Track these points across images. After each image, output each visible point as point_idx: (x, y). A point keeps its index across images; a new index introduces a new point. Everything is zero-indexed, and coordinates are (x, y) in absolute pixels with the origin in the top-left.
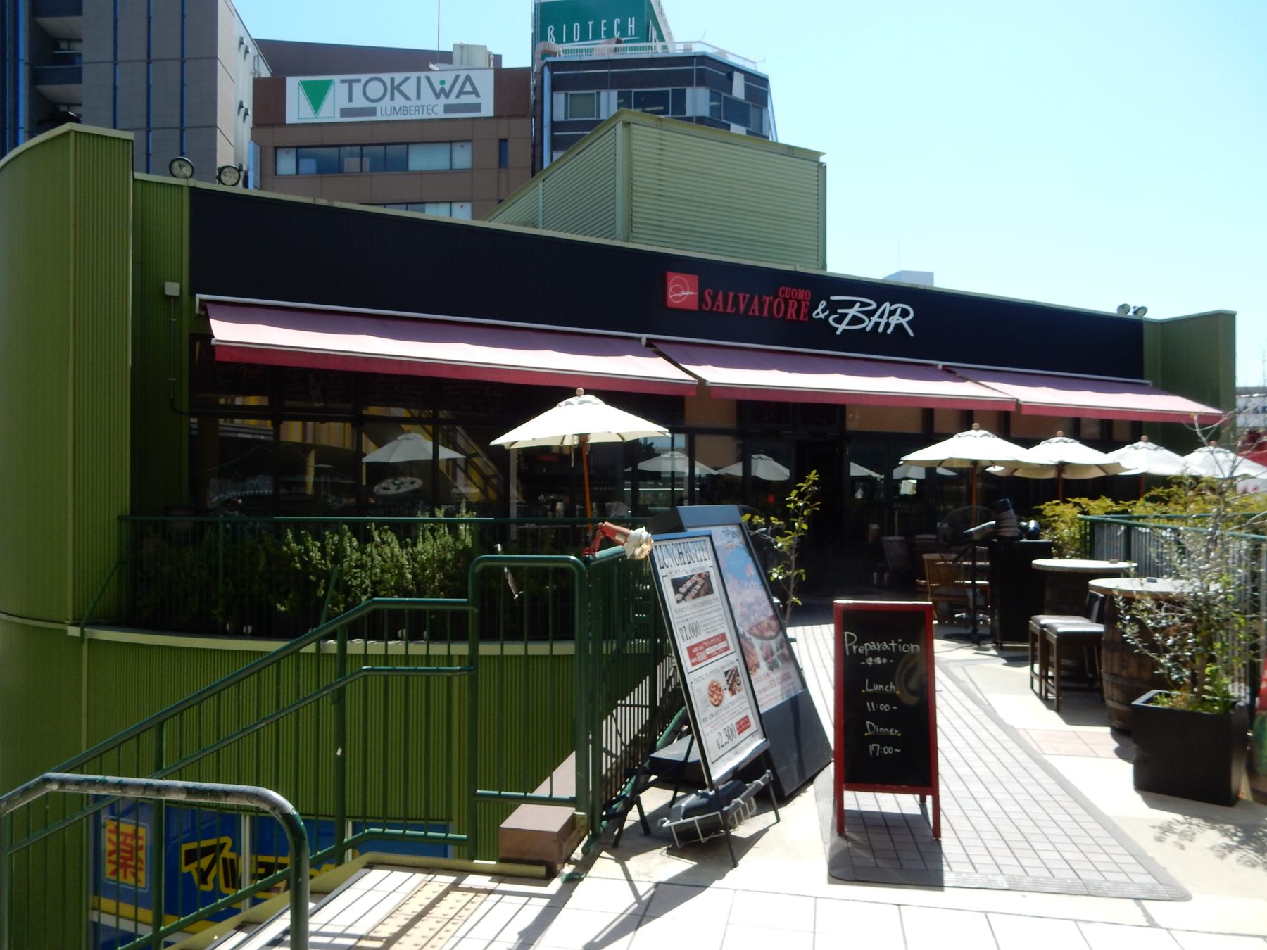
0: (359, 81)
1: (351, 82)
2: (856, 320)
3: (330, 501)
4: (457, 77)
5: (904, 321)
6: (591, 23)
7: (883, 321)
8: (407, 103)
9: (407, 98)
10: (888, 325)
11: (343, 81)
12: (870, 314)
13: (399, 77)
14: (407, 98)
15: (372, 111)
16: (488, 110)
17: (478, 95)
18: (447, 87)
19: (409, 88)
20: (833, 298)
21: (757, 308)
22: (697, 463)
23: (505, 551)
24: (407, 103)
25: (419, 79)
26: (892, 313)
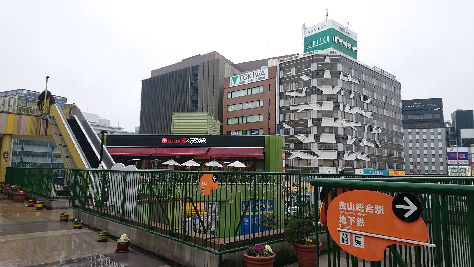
0: (242, 75)
1: (241, 76)
2: (194, 142)
4: (261, 71)
5: (204, 141)
6: (317, 40)
7: (200, 141)
8: (251, 79)
9: (251, 78)
10: (201, 142)
11: (239, 76)
12: (197, 141)
13: (250, 73)
14: (251, 78)
15: (245, 82)
16: (267, 78)
17: (265, 75)
18: (259, 74)
19: (251, 76)
20: (190, 139)
23: (451, 183)
24: (251, 79)
25: (253, 73)
26: (202, 140)
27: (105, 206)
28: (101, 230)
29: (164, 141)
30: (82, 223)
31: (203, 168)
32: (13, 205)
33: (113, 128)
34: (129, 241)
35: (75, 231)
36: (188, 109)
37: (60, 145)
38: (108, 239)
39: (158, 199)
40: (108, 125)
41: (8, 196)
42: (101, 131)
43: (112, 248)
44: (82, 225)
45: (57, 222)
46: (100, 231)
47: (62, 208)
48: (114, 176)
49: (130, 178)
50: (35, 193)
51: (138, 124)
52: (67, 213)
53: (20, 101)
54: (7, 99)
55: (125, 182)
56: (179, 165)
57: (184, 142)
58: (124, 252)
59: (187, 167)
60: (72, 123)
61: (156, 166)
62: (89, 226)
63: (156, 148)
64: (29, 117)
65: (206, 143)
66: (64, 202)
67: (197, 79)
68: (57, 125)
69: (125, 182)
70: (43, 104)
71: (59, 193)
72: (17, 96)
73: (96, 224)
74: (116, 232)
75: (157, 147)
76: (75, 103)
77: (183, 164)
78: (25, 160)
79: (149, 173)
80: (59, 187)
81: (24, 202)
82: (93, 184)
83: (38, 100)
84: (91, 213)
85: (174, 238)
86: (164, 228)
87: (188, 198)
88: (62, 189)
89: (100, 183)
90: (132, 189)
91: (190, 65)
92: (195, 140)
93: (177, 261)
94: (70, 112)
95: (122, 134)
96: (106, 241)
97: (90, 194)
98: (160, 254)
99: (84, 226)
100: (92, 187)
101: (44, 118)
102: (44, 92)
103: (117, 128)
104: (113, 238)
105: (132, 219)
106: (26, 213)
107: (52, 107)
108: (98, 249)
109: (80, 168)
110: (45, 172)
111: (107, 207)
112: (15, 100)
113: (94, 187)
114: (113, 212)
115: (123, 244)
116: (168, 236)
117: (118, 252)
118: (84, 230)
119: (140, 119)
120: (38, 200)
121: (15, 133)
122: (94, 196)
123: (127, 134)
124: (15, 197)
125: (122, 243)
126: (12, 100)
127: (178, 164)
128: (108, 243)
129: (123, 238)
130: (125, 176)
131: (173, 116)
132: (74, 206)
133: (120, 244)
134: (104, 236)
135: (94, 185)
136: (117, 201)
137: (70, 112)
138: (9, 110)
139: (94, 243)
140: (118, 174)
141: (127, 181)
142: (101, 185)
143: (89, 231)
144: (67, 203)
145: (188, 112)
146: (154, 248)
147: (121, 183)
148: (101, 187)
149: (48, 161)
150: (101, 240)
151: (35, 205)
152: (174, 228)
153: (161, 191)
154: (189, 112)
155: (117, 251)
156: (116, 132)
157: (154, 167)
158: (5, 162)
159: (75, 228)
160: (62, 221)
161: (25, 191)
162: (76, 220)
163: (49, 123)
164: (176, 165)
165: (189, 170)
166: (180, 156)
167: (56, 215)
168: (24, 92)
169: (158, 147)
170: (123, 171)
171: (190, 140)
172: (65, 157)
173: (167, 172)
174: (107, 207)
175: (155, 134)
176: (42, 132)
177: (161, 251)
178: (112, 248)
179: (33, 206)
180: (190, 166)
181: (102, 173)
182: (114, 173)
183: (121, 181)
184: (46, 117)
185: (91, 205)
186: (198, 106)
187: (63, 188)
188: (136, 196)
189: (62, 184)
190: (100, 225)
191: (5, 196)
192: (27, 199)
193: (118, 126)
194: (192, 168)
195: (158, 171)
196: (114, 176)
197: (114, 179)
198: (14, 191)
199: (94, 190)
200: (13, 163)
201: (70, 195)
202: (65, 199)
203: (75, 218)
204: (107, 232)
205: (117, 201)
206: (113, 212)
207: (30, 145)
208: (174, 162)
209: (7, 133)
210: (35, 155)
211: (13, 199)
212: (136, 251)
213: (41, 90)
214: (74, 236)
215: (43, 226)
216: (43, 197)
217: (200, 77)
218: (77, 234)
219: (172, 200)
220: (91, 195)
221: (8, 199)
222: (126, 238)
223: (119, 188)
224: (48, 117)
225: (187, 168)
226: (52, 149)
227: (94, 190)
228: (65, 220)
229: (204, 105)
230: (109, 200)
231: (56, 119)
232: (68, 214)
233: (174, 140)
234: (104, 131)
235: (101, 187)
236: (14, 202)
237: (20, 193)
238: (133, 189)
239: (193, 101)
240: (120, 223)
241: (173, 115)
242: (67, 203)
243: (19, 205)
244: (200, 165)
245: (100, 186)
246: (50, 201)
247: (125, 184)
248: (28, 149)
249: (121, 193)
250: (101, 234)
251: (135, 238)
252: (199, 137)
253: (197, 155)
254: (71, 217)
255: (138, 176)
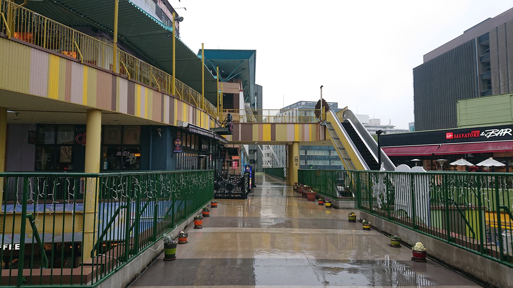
2: (492, 134)
3: (239, 212)
5: (508, 132)
10: (503, 134)
20: (486, 131)
21: (466, 136)
22: (460, 235)
27: (392, 210)
28: (391, 234)
29: (449, 136)
30: (370, 225)
31: (510, 169)
32: (307, 203)
33: (385, 127)
34: (426, 251)
35: (364, 232)
36: (478, 92)
37: (338, 149)
38: (400, 244)
39: (457, 207)
40: (379, 124)
41: (302, 195)
42: (376, 132)
43: (406, 255)
44: (371, 227)
45: (345, 221)
46: (390, 235)
47: (348, 209)
48: (399, 178)
49: (418, 180)
50: (322, 193)
51: (412, 120)
52: (354, 214)
53: (300, 112)
54: (291, 111)
55: (412, 185)
56: (473, 165)
57: (478, 136)
58: (423, 262)
59: (485, 168)
60: (347, 126)
61: (442, 167)
62: (377, 229)
63: (439, 146)
64: (310, 125)
65: (511, 135)
66: (349, 202)
67: (489, 51)
68: (333, 130)
69: (412, 185)
70: (320, 112)
71: (341, 193)
72: (297, 109)
73: (385, 227)
74: (408, 239)
75: (440, 144)
76: (347, 107)
77: (479, 164)
78: (309, 163)
79: (439, 176)
80: (341, 188)
81: (315, 200)
82: (377, 186)
83: (315, 109)
84: (378, 216)
85: (485, 255)
86: (470, 241)
87: (502, 208)
88: (343, 190)
89: (384, 185)
90: (422, 193)
91: (475, 36)
92: (493, 132)
93: (493, 284)
94: (343, 116)
95: (394, 133)
96: (398, 246)
97: (375, 196)
98: (467, 271)
99: (372, 228)
100: (376, 189)
101: (322, 124)
102: (320, 101)
103: (388, 127)
104: (405, 245)
105: (426, 227)
106: (317, 210)
107: (328, 113)
108: (391, 254)
109: (358, 169)
110: (329, 174)
111: (395, 210)
112: (296, 112)
113: (379, 189)
114: (399, 216)
115: (419, 252)
116: (476, 252)
117: (414, 260)
118: (373, 233)
119: (414, 113)
120: (326, 199)
121: (301, 141)
122: (379, 198)
123: (401, 133)
124: (308, 196)
125: (418, 251)
126: (294, 111)
127: (470, 164)
128: (401, 249)
129: (419, 246)
130: (412, 179)
131: (458, 105)
132: (360, 207)
133: (416, 252)
134: (396, 241)
135: (378, 187)
136: (405, 205)
137: (343, 116)
138: (289, 122)
139: (384, 246)
140: (403, 177)
141: (414, 184)
142: (386, 187)
143: (379, 234)
144: (352, 204)
145: (478, 96)
146: (458, 262)
147: (408, 186)
148: (386, 190)
149: (327, 163)
150: (392, 245)
151: (324, 204)
152: (485, 243)
153: (461, 197)
154: (479, 96)
155: (413, 259)
156: (387, 130)
157: (438, 168)
158: (296, 165)
159: (364, 229)
160: (350, 221)
161: (314, 191)
162: (364, 221)
163: (326, 128)
164: (468, 166)
165: (488, 171)
166: (472, 154)
167: (343, 215)
168: (303, 103)
169: (441, 145)
170: (408, 173)
171: (486, 133)
172: (344, 159)
173: (467, 174)
174: (395, 210)
175: (434, 129)
176: (322, 138)
177: (468, 268)
178: (406, 255)
179: (322, 204)
180: (490, 167)
181: (384, 175)
182: (399, 175)
183: (408, 184)
184: (324, 123)
185: (378, 207)
186: (493, 86)
187: (345, 189)
188: (427, 202)
189: (342, 185)
190: (389, 229)
191: (300, 194)
192: (317, 198)
193: (389, 125)
194: (493, 168)
195: (454, 173)
196: (399, 178)
197: (399, 181)
198: (306, 190)
199: (379, 192)
200: (301, 166)
201: (351, 196)
202: (350, 199)
203: (362, 219)
204: (398, 237)
205: (405, 205)
206: (399, 216)
207: (311, 150)
208: (465, 162)
209: (296, 141)
210: (316, 158)
211: (306, 197)
212: (433, 262)
213: (316, 99)
214: (364, 237)
215: (333, 224)
216: (330, 197)
217: (492, 48)
218: (367, 235)
219: (477, 208)
220: (376, 198)
221: (303, 197)
222: (421, 246)
223: (406, 191)
224: (325, 123)
225: (485, 169)
226: (329, 152)
227: (379, 192)
228: (353, 220)
229: (502, 84)
230: (396, 204)
231: (333, 124)
232: (356, 214)
233: (462, 134)
234: (379, 131)
235: (386, 190)
236: (308, 200)
237: (311, 192)
238: (423, 194)
239: (483, 80)
240: (412, 230)
241: (458, 104)
242: (352, 204)
243: (311, 203)
244: (504, 165)
245: (384, 188)
246: (336, 201)
247: (412, 187)
248: (310, 153)
249: (409, 197)
250: (392, 238)
251: (431, 249)
252: (500, 128)
253: (499, 152)
254: (358, 218)
255: (428, 179)
